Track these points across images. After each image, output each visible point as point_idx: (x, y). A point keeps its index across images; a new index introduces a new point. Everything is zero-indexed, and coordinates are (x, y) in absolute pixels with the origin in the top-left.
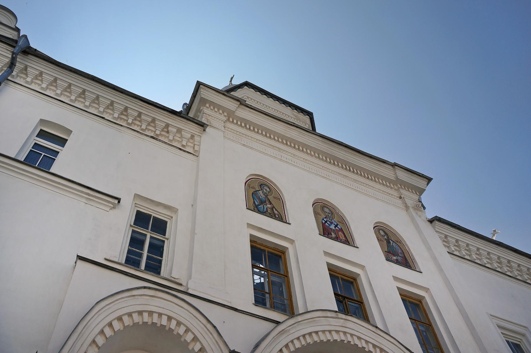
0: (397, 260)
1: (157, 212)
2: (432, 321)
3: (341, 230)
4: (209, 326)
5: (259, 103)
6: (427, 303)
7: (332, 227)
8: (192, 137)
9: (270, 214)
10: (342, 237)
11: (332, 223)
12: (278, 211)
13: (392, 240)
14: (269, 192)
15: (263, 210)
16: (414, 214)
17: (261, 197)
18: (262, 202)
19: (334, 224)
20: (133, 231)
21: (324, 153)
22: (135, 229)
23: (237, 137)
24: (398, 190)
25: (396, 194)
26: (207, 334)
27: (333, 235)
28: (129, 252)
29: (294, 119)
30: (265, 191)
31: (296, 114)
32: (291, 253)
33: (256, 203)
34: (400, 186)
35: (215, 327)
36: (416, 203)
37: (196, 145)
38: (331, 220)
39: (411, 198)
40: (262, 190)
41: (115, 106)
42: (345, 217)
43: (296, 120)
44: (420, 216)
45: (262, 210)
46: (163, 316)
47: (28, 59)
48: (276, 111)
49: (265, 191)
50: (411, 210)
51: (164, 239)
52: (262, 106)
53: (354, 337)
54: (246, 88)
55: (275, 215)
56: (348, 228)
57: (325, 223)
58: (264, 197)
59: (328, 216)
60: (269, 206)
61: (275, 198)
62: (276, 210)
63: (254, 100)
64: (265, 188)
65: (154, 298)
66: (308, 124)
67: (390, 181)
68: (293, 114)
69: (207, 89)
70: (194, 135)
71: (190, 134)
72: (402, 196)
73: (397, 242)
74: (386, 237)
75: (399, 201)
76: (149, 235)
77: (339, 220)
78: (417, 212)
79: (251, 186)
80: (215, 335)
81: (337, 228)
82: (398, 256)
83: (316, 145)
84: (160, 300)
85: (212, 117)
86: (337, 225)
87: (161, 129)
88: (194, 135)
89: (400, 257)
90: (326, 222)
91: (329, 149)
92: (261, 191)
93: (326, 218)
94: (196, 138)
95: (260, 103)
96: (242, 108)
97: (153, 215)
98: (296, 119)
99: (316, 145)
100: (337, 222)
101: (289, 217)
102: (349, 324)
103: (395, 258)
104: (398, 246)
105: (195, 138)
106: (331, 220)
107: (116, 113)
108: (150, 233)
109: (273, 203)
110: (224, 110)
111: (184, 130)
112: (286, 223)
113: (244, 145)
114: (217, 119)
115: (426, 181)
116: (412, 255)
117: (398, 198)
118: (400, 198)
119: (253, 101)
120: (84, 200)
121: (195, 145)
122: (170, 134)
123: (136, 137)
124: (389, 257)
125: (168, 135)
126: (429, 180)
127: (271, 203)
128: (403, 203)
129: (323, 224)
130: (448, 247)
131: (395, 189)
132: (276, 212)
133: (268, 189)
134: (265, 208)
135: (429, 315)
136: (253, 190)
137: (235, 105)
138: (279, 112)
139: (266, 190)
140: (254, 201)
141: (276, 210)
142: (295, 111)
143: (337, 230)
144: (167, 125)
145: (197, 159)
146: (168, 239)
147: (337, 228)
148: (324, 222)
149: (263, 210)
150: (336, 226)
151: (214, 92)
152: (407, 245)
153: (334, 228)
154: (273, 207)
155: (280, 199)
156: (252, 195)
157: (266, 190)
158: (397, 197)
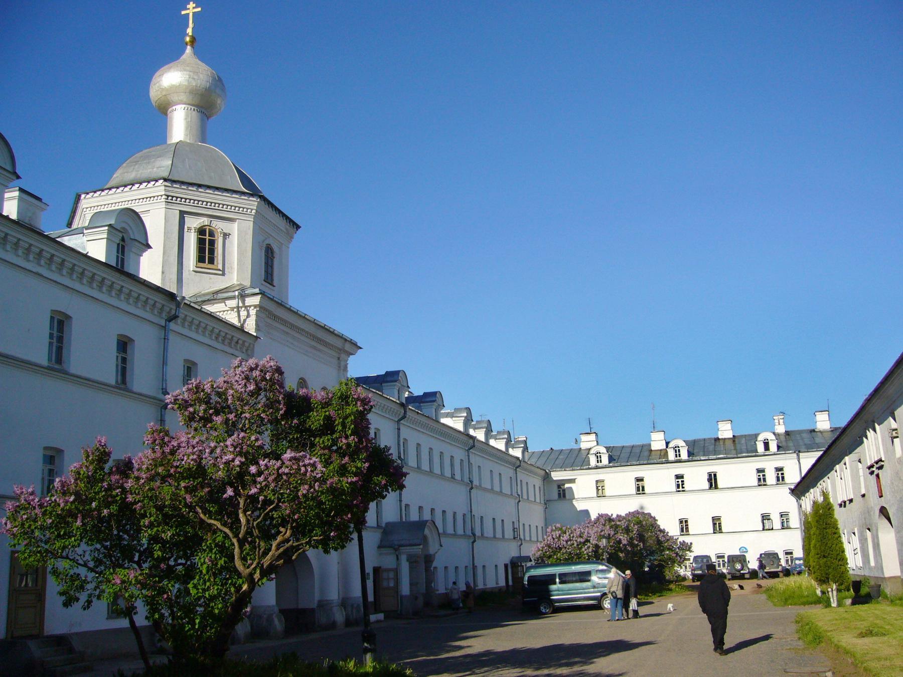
25: (336, 355)
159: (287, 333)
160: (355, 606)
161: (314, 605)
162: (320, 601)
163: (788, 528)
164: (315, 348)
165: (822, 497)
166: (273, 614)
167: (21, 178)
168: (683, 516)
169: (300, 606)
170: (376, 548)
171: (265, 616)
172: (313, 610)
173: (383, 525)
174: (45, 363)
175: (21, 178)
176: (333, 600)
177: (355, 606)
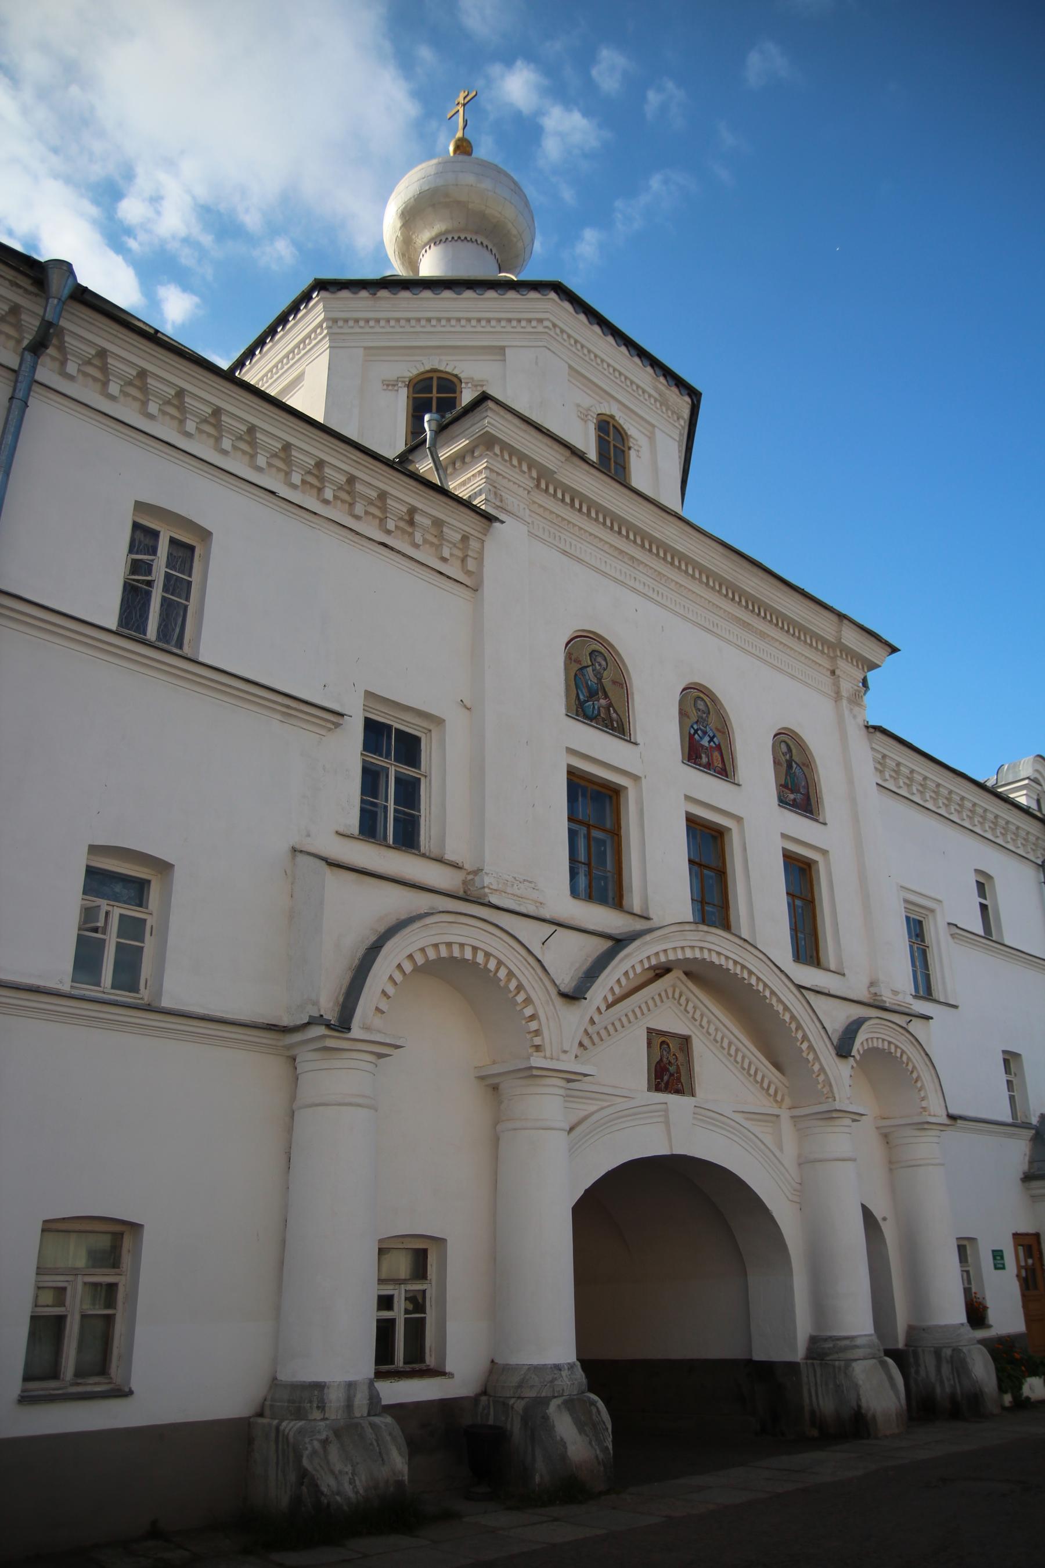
0: (794, 800)
1: (404, 720)
2: (816, 897)
3: (719, 747)
4: (531, 960)
5: (579, 346)
6: (818, 871)
7: (705, 742)
8: (465, 538)
9: (604, 720)
10: (718, 763)
11: (705, 733)
12: (617, 714)
13: (796, 763)
14: (605, 670)
15: (593, 712)
16: (846, 713)
17: (589, 682)
18: (592, 695)
19: (709, 735)
20: (364, 761)
21: (717, 577)
22: (367, 759)
23: (552, 530)
24: (833, 659)
25: (826, 663)
26: (527, 969)
27: (704, 760)
28: (363, 801)
29: (656, 400)
30: (598, 667)
31: (663, 388)
32: (632, 795)
33: (581, 697)
34: (839, 654)
35: (539, 961)
36: (856, 688)
37: (470, 556)
38: (706, 727)
39: (849, 673)
40: (593, 664)
41: (295, 457)
42: (730, 720)
43: (658, 405)
44: (855, 717)
45: (589, 712)
46: (466, 947)
47: (73, 314)
48: (617, 374)
49: (598, 667)
50: (845, 702)
51: (418, 776)
52: (584, 354)
53: (712, 952)
54: (553, 300)
55: (612, 721)
56: (730, 743)
57: (694, 734)
58: (596, 681)
59: (702, 718)
60: (603, 702)
61: (614, 682)
62: (615, 711)
63: (569, 336)
64: (599, 659)
65: (452, 924)
66: (683, 418)
67: (824, 642)
68: (656, 389)
69: (502, 412)
70: (469, 536)
71: (459, 533)
72: (838, 672)
73: (804, 764)
74: (788, 757)
75: (827, 680)
76: (393, 769)
77: (719, 727)
78: (852, 707)
79: (573, 658)
80: (539, 970)
81: (712, 744)
82: (798, 792)
83: (709, 561)
84: (461, 925)
85: (504, 477)
86: (714, 736)
87: (397, 516)
88: (469, 536)
89: (801, 794)
90: (696, 731)
91: (731, 571)
92: (591, 668)
93: (697, 722)
94: (474, 544)
95: (583, 346)
96: (573, 463)
97: (396, 725)
98: (660, 401)
99: (709, 561)
100: (714, 730)
101: (637, 727)
102: (709, 938)
103: (792, 796)
104: (804, 773)
105: (471, 543)
106: (706, 727)
107: (295, 471)
108: (395, 766)
109: (610, 694)
110: (532, 464)
111: (448, 523)
112: (630, 741)
113: (565, 553)
114: (515, 483)
115: (887, 651)
116: (821, 792)
117: (829, 672)
118: (833, 673)
119: (565, 336)
120: (279, 717)
121: (467, 556)
122: (417, 529)
123: (346, 540)
124: (784, 796)
125: (410, 530)
126: (894, 650)
127: (606, 696)
128: (834, 684)
129: (691, 737)
130: (881, 772)
131: (828, 656)
132: (614, 716)
133: (603, 663)
134: (596, 707)
135: (815, 887)
136: (578, 666)
137: (558, 456)
138: (623, 378)
139: (600, 665)
140: (578, 694)
141: (615, 711)
142: (662, 379)
143: (711, 747)
144: (412, 511)
145: (473, 596)
146: (426, 776)
147: (712, 744)
148: (692, 731)
149: (593, 712)
150: (711, 740)
151: (517, 421)
152: (817, 771)
153: (707, 744)
154: (610, 705)
155: (622, 684)
156: (575, 679)
157: (600, 665)
158: (828, 669)
159: (621, 552)
160: (947, 1352)
161: (799, 1354)
162: (813, 1340)
163: (294, 857)
164: (746, 625)
165: (425, 1368)
166: (544, 1402)
167: (899, 650)
168: (959, 1008)
169: (759, 1355)
170: (1020, 1182)
171: (519, 1406)
172: (792, 1367)
173: (1034, 1121)
174: (113, 624)
175: (899, 650)
176: (852, 1338)
177: (947, 1352)
